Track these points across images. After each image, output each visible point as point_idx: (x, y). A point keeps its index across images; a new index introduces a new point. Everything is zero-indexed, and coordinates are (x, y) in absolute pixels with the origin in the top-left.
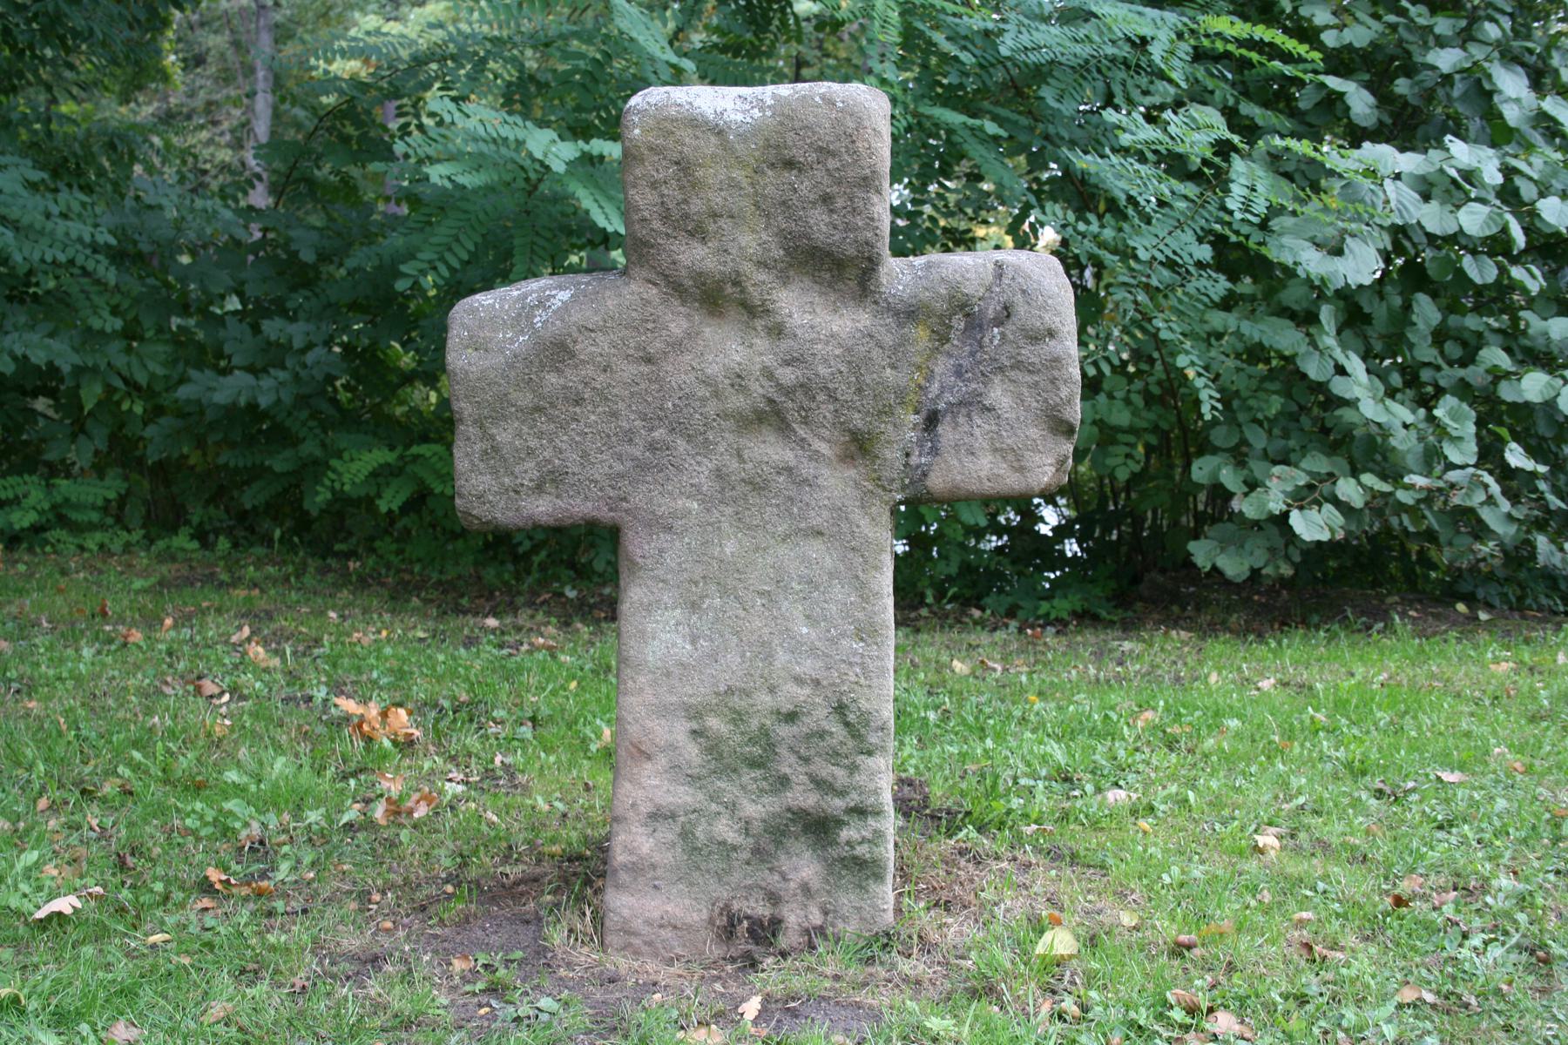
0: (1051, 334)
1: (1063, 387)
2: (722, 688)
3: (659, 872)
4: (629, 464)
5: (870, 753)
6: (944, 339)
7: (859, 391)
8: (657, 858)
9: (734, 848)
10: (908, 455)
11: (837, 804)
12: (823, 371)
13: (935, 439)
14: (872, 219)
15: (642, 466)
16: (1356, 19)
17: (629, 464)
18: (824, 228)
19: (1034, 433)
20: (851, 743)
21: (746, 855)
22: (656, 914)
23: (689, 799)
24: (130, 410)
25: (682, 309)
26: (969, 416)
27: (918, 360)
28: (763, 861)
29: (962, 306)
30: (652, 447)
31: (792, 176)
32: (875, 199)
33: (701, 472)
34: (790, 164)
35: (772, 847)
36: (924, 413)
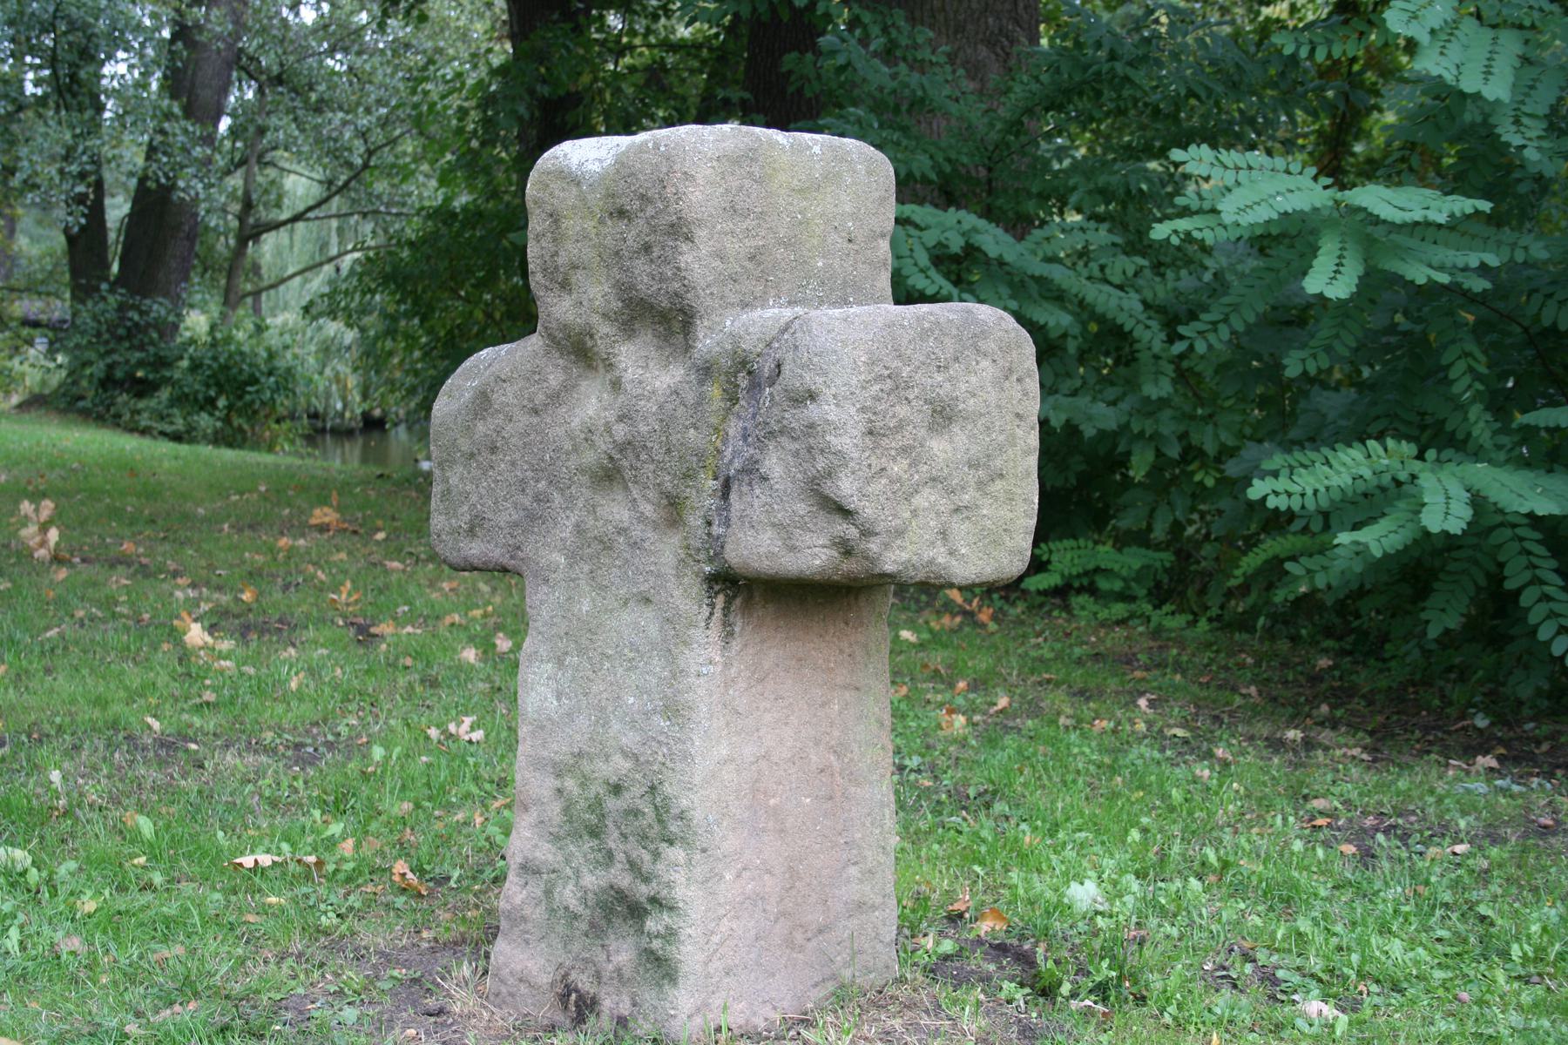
0: (812, 396)
1: (820, 458)
2: (576, 750)
3: (529, 926)
4: (522, 513)
5: (671, 843)
6: (734, 400)
7: (669, 451)
8: (527, 911)
9: (576, 917)
10: (709, 524)
11: (643, 891)
12: (643, 428)
13: (727, 508)
14: (679, 269)
15: (532, 517)
16: (283, 169)
17: (522, 513)
18: (646, 279)
19: (802, 508)
20: (657, 828)
21: (584, 926)
22: (519, 967)
23: (550, 857)
24: (1372, 366)
25: (561, 362)
26: (750, 484)
27: (714, 420)
28: (598, 937)
29: (744, 363)
30: (537, 499)
31: (622, 225)
32: (684, 247)
33: (565, 530)
34: (621, 213)
35: (603, 922)
36: (721, 479)
